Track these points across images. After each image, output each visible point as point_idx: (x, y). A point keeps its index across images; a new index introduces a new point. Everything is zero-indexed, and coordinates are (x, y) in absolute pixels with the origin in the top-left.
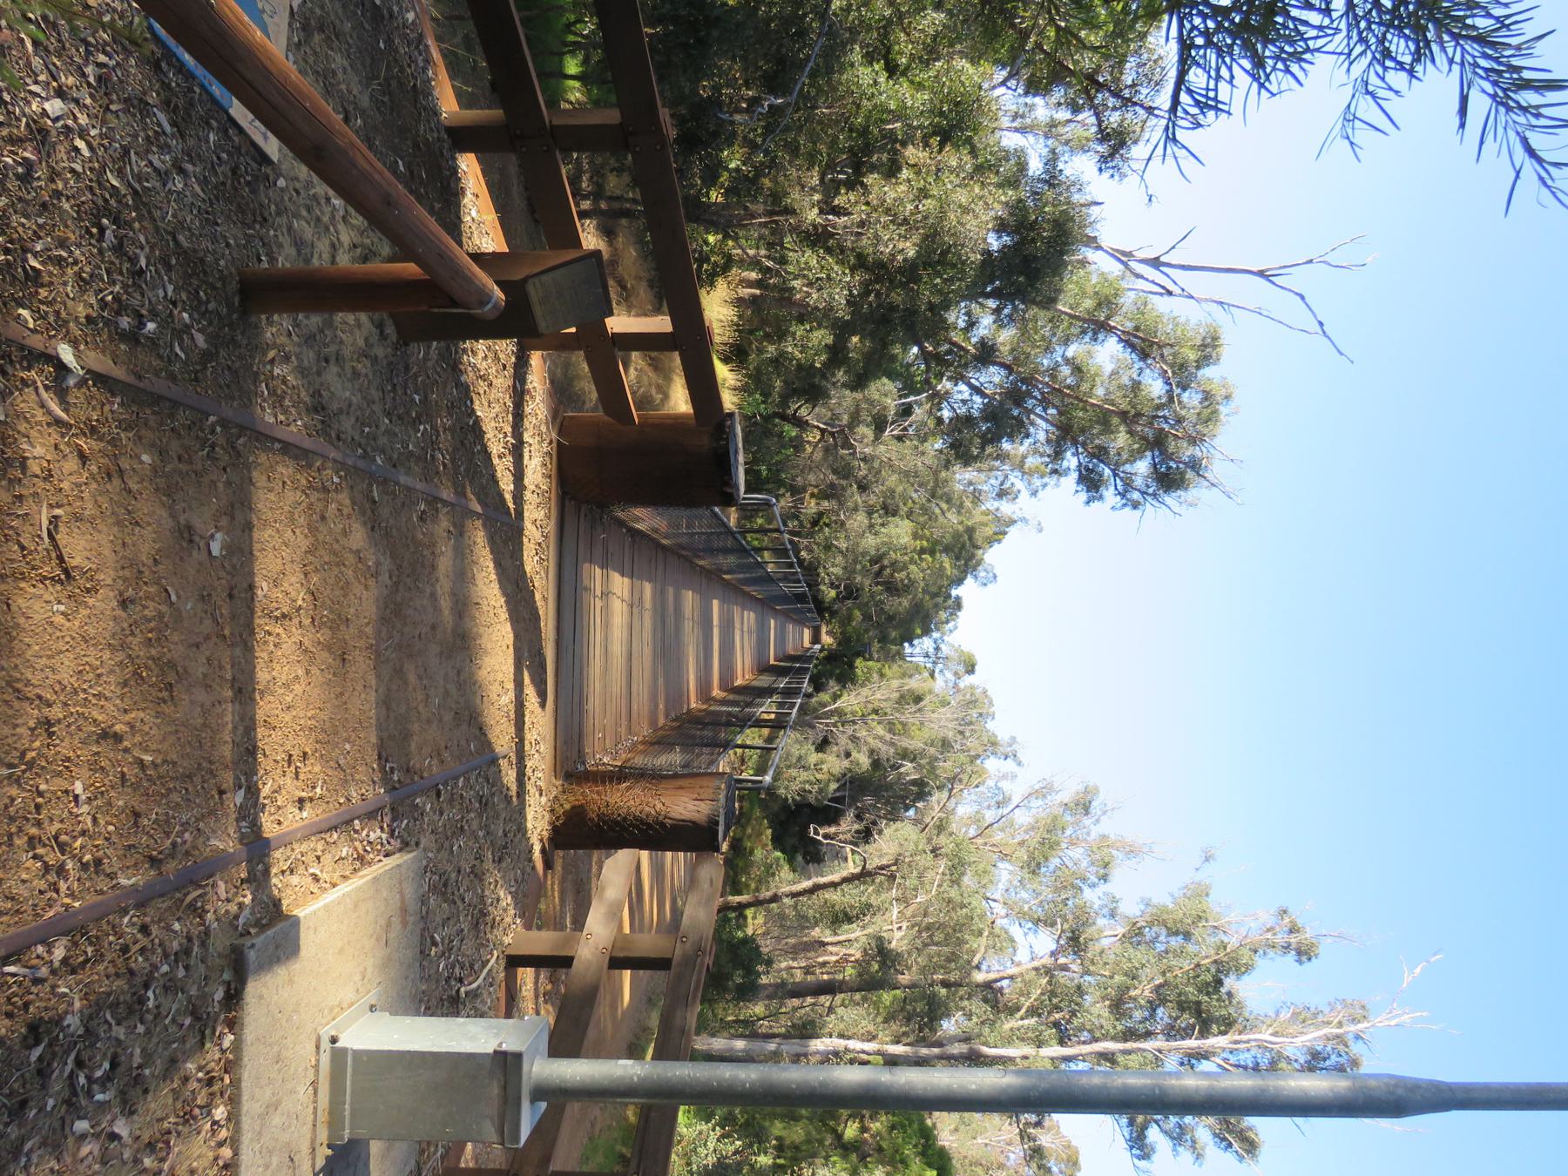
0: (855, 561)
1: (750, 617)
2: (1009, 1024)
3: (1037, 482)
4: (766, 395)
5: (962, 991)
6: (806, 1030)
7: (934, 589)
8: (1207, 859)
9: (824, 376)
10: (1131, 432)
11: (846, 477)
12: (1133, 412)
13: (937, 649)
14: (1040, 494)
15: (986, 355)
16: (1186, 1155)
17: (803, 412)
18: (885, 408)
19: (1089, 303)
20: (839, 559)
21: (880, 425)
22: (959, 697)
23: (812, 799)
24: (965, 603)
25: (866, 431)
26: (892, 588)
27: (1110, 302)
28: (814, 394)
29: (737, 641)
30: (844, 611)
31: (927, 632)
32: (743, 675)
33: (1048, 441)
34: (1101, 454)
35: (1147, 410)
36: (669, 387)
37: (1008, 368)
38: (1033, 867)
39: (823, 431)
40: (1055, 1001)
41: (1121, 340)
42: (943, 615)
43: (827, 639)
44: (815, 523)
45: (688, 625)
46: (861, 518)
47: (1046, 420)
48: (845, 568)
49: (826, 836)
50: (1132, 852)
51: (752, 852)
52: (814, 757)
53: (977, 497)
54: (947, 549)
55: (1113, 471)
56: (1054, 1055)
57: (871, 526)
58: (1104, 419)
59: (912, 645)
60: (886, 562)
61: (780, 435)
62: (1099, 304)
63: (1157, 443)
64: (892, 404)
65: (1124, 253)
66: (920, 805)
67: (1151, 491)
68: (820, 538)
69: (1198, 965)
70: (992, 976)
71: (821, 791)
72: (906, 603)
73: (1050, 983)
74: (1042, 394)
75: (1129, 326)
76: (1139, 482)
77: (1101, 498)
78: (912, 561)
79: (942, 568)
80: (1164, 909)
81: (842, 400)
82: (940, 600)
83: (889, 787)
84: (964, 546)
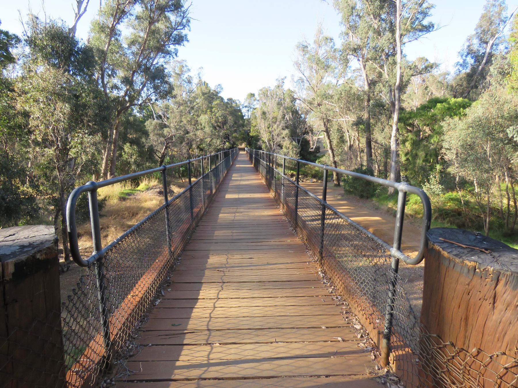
0: (215, 135)
1: (235, 176)
2: (385, 76)
3: (185, 69)
5: (371, 95)
6: (387, 151)
7: (225, 108)
10: (158, 21)
11: (184, 138)
13: (246, 107)
14: (189, 68)
15: (128, 81)
16: (431, 11)
17: (160, 155)
19: (103, 36)
20: (214, 141)
21: (163, 126)
22: (263, 99)
23: (298, 150)
24: (230, 97)
25: (166, 131)
26: (225, 123)
27: (102, 27)
29: (245, 179)
30: (233, 139)
31: (240, 111)
32: (260, 180)
33: (164, 57)
34: (168, 35)
35: (148, 13)
36: (145, 208)
38: (326, 67)
40: (378, 58)
41: (118, 23)
42: (234, 105)
43: (243, 146)
44: (201, 150)
45: (239, 217)
46: (199, 133)
47: (155, 58)
48: (217, 139)
49: (313, 145)
50: (320, 32)
51: (316, 171)
52: (284, 150)
53: (191, 91)
54: (210, 102)
57: (202, 129)
58: (152, 33)
59: (244, 116)
60: (216, 125)
65: (76, 16)
66: (300, 113)
67: (182, 15)
68: (206, 148)
70: (366, 83)
72: (230, 117)
73: (371, 60)
74: (144, 59)
76: (179, 19)
77: (186, 35)
78: (215, 115)
79: (217, 104)
80: (343, 17)
81: (153, 140)
82: (229, 106)
83: (294, 124)
84: (209, 96)
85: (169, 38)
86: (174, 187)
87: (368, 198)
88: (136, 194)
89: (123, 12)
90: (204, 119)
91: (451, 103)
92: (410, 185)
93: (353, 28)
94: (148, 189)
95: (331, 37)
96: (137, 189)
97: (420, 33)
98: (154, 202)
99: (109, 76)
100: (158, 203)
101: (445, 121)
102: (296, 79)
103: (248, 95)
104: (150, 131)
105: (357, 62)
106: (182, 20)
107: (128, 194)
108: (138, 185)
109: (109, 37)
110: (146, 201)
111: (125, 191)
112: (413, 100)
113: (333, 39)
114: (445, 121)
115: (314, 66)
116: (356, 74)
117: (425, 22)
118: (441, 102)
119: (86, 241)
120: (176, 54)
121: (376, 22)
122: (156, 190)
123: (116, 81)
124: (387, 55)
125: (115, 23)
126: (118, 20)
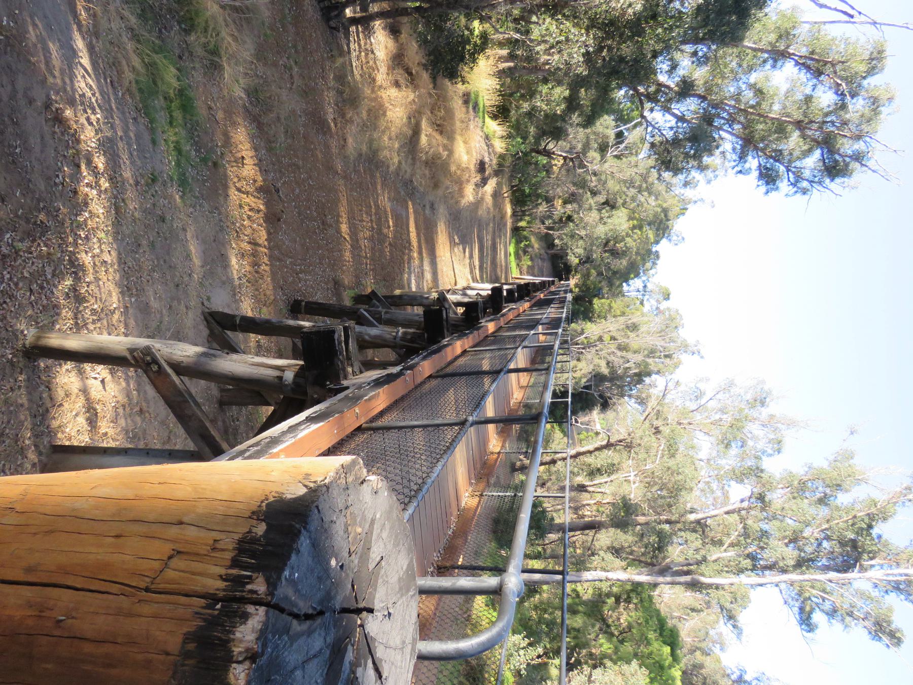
2: (715, 554)
4: (525, 138)
5: (679, 526)
8: (852, 433)
9: (564, 120)
10: (804, 137)
11: (583, 187)
12: (807, 120)
13: (645, 287)
14: (712, 183)
15: (686, 89)
17: (551, 146)
18: (607, 137)
21: (603, 149)
24: (661, 254)
25: (593, 155)
26: (615, 253)
27: (788, 34)
28: (558, 133)
33: (734, 149)
34: (778, 156)
37: (703, 98)
39: (565, 158)
41: (797, 63)
46: (595, 215)
48: (585, 249)
55: (787, 167)
56: (753, 583)
57: (601, 218)
58: (781, 129)
61: (536, 164)
62: (780, 37)
63: (827, 143)
64: (611, 134)
67: (816, 179)
69: (855, 517)
71: (577, 383)
73: (744, 528)
74: (730, 114)
75: (804, 51)
76: (807, 174)
77: (777, 189)
81: (577, 135)
84: (661, 221)
85: (771, 157)
86: (494, 185)
87: (495, 532)
88: (477, 119)
89: (818, 73)
90: (620, 221)
91: (673, 670)
92: (522, 601)
93: (800, 488)
94: (487, 138)
95: (783, 450)
96: (486, 116)
97: (797, 609)
98: (465, 158)
99: (695, 54)
100: (463, 165)
101: (641, 667)
102: (702, 386)
103: (667, 290)
104: (594, 128)
105: (739, 499)
106: (807, 180)
107: (476, 106)
108: (494, 117)
109: (770, 49)
110: (465, 142)
111: (480, 99)
112: (670, 597)
113: (779, 452)
114: (641, 667)
115: (728, 418)
116: (715, 496)
117: (818, 617)
118: (673, 653)
119: (386, 48)
120: (740, 172)
121: (815, 534)
122: (486, 155)
123: (685, 64)
124: (752, 557)
125: (796, 58)
126: (803, 64)
